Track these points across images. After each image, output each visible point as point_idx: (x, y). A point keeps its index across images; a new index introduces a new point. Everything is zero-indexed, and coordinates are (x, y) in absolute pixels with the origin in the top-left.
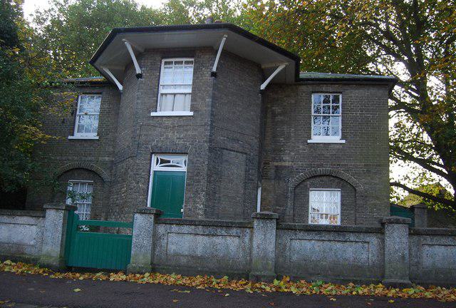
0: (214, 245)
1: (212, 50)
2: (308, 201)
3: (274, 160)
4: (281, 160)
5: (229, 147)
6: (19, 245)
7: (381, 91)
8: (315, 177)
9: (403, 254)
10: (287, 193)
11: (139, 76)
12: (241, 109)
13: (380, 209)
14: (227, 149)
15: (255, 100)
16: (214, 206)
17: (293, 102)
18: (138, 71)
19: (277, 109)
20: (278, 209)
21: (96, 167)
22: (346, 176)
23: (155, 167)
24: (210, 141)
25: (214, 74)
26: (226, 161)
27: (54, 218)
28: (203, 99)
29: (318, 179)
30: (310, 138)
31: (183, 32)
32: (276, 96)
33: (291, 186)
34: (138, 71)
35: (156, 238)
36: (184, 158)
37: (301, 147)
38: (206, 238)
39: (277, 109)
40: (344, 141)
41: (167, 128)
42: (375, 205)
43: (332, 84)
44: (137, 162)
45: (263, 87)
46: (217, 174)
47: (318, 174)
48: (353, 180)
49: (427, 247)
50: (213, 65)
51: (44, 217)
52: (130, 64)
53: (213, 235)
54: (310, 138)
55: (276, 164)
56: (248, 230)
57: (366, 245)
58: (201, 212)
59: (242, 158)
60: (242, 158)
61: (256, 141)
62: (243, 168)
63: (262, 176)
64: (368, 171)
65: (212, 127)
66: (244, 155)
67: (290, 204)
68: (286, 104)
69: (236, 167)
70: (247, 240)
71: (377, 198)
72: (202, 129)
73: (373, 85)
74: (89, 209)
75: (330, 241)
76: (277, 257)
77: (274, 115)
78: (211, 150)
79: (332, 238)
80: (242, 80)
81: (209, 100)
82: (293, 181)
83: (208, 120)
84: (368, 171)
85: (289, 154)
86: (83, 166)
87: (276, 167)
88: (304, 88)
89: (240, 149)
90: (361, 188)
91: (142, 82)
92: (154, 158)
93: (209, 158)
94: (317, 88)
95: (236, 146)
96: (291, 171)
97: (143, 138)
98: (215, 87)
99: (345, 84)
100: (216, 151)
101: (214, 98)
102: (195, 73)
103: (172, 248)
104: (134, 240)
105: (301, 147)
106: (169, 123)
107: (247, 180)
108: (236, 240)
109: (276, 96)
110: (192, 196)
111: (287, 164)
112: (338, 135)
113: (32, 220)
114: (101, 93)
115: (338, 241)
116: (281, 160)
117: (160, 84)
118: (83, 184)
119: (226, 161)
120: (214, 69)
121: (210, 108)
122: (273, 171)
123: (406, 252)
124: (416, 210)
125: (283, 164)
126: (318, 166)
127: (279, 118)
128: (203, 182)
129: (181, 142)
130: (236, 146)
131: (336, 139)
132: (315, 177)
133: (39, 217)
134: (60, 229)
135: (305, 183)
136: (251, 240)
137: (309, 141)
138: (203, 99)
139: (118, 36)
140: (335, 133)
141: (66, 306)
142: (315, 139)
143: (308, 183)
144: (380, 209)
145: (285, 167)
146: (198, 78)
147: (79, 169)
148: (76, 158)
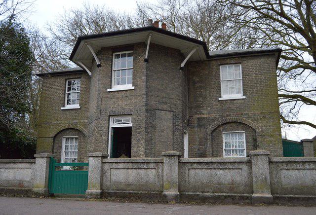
0: (139, 174)
1: (143, 45)
3: (196, 113)
4: (201, 113)
5: (160, 108)
6: (21, 183)
7: (270, 59)
8: (225, 124)
9: (265, 177)
11: (99, 66)
12: (167, 82)
13: (274, 144)
14: (159, 110)
16: (151, 149)
17: (207, 72)
18: (98, 63)
21: (80, 127)
22: (248, 122)
23: (114, 125)
24: (146, 105)
25: (146, 61)
26: (159, 117)
27: (41, 164)
28: (140, 77)
29: (228, 126)
30: (220, 97)
31: (126, 35)
33: (209, 131)
34: (98, 63)
35: (103, 172)
36: (130, 118)
37: (214, 103)
38: (135, 171)
40: (244, 97)
41: (118, 98)
42: (271, 141)
43: (233, 58)
44: (101, 122)
45: (182, 65)
47: (228, 121)
48: (253, 125)
49: (284, 171)
50: (145, 54)
51: (35, 163)
52: (94, 60)
53: (139, 169)
54: (220, 97)
55: (198, 116)
56: (160, 164)
57: (240, 171)
58: (142, 153)
59: (170, 115)
60: (170, 115)
61: (179, 102)
62: (171, 121)
63: (189, 124)
65: (147, 96)
66: (172, 113)
67: (209, 143)
68: (202, 74)
69: (165, 121)
70: (160, 170)
71: (272, 136)
72: (140, 98)
74: (77, 155)
75: (215, 169)
76: (179, 181)
77: (194, 83)
78: (147, 111)
79: (216, 167)
80: (167, 62)
81: (144, 78)
82: (210, 128)
83: (144, 91)
84: (264, 117)
86: (71, 126)
87: (198, 118)
88: (214, 62)
89: (168, 109)
91: (100, 70)
92: (111, 119)
93: (146, 117)
94: (223, 62)
95: (165, 107)
96: (208, 121)
97: (103, 106)
98: (148, 69)
99: (242, 57)
100: (151, 111)
101: (147, 76)
102: (134, 60)
103: (114, 178)
104: (89, 174)
105: (214, 103)
106: (119, 95)
107: (175, 130)
108: (154, 171)
109: (195, 70)
110: (136, 142)
112: (241, 93)
113: (27, 165)
114: (80, 78)
115: (221, 169)
116: (201, 113)
117: (113, 69)
118: (72, 139)
119: (159, 117)
120: (146, 57)
121: (145, 83)
122: (196, 122)
123: (268, 175)
124: (304, 144)
125: (203, 116)
126: (227, 116)
127: (198, 85)
128: (143, 133)
129: (128, 107)
130: (165, 107)
131: (240, 96)
132: (225, 124)
133: (32, 163)
134: (45, 170)
135: (219, 129)
136: (163, 170)
137: (220, 99)
138: (140, 77)
139: (82, 43)
140: (238, 93)
142: (225, 97)
143: (221, 128)
144: (274, 144)
145: (204, 118)
146: (136, 64)
147: (68, 129)
148: (66, 122)
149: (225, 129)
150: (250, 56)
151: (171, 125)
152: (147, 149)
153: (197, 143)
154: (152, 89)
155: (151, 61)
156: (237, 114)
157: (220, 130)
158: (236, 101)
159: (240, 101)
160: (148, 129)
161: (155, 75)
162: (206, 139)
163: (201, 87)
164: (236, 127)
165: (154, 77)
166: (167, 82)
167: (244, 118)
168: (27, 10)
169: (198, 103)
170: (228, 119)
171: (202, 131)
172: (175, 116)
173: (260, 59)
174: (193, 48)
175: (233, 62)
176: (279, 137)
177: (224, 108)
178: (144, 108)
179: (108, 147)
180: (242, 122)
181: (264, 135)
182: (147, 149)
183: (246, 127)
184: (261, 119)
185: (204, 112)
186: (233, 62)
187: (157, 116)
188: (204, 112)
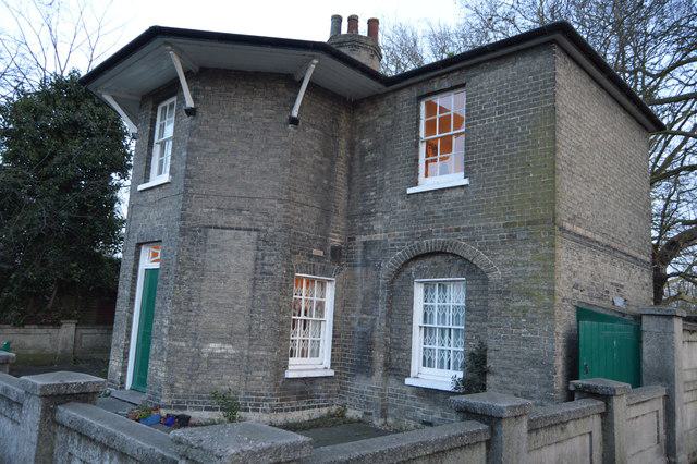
2: (412, 304)
4: (372, 231)
10: (378, 289)
12: (247, 158)
13: (533, 320)
15: (278, 138)
17: (389, 123)
19: (367, 142)
20: (364, 319)
22: (469, 250)
24: (183, 218)
26: (214, 246)
32: (367, 120)
39: (367, 142)
42: (524, 310)
46: (195, 269)
47: (424, 250)
48: (482, 259)
55: (364, 238)
59: (248, 239)
60: (248, 239)
62: (251, 254)
64: (512, 237)
66: (255, 234)
67: (381, 309)
68: (378, 129)
71: (528, 295)
72: (175, 202)
73: (522, 52)
77: (364, 153)
78: (183, 232)
82: (388, 266)
85: (382, 218)
87: (365, 243)
89: (246, 224)
90: (496, 276)
95: (235, 219)
99: (468, 68)
111: (379, 237)
116: (372, 231)
119: (214, 246)
122: (359, 252)
125: (373, 237)
126: (424, 235)
127: (369, 157)
130: (235, 219)
131: (458, 179)
141: (123, 455)
142: (427, 184)
145: (376, 242)
149: (421, 273)
150: (488, 61)
151: (250, 264)
152: (177, 322)
153: (358, 307)
154: (202, 178)
155: (203, 114)
156: (446, 231)
157: (410, 275)
158: (447, 194)
159: (455, 194)
160: (183, 273)
161: (214, 144)
162: (377, 298)
163: (374, 163)
164: (445, 266)
165: (210, 150)
166: (247, 158)
167: (461, 241)
168: (93, 39)
169: (367, 203)
170: (428, 244)
171: (370, 275)
172: (265, 241)
173: (535, 57)
174: (309, 61)
175: (446, 84)
176: (547, 300)
177: (419, 214)
178: (178, 224)
179: (132, 313)
180: (455, 252)
181: (507, 292)
182: (177, 322)
183: (469, 269)
184: (503, 243)
185: (378, 226)
186: (446, 84)
187: (210, 242)
188: (378, 226)
